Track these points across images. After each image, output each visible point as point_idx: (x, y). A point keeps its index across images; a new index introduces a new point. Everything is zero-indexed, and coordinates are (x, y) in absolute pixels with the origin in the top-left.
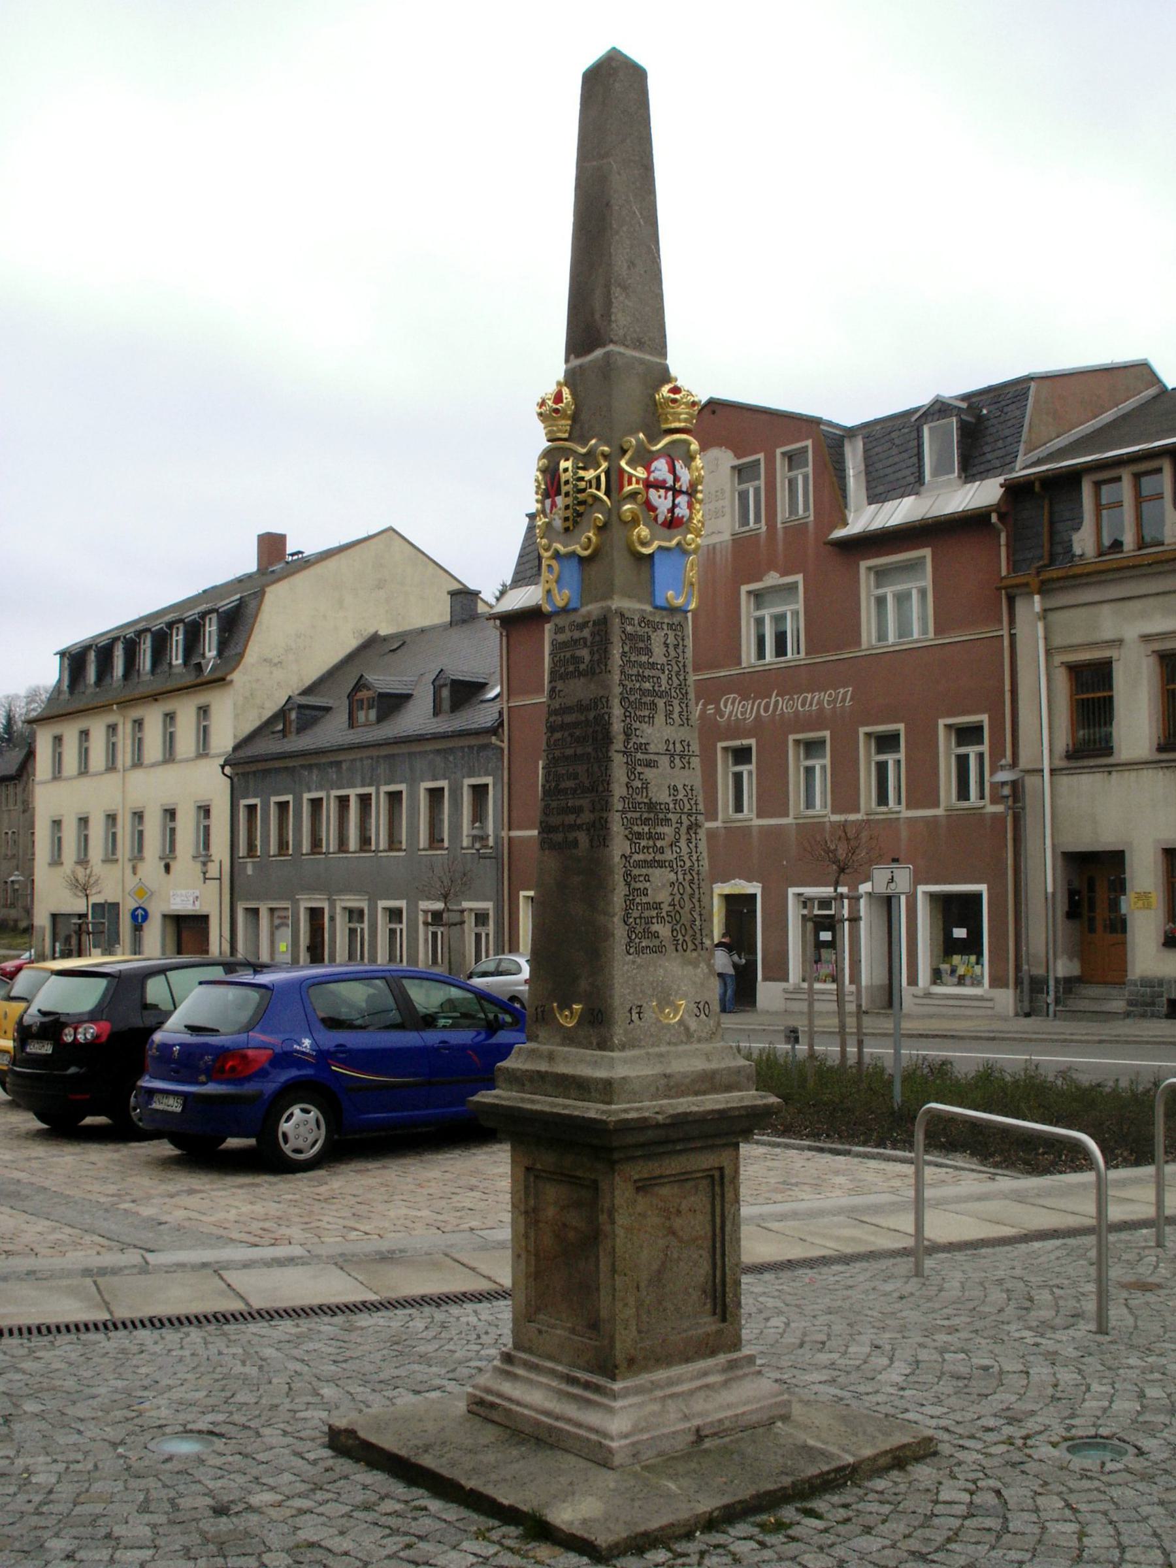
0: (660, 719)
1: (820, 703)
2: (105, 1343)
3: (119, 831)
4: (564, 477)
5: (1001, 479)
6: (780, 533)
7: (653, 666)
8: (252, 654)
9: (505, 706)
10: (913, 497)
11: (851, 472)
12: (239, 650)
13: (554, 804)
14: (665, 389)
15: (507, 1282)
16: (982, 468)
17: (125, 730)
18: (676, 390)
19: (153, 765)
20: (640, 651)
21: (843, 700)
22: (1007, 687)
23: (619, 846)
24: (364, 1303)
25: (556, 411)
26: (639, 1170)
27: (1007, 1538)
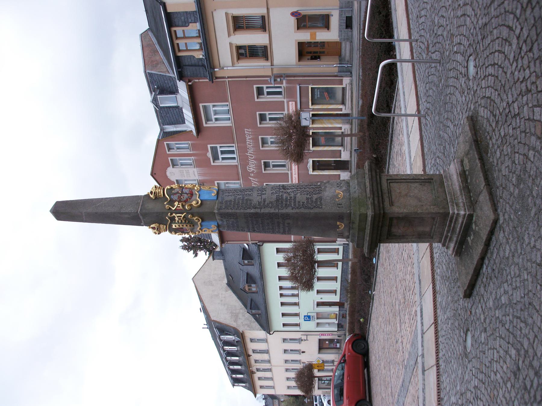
0: (251, 198)
1: (250, 139)
2: (443, 367)
3: (291, 368)
4: (177, 227)
5: (178, 81)
6: (194, 152)
7: (235, 200)
8: (233, 324)
9: (250, 242)
10: (183, 110)
11: (175, 129)
12: (232, 329)
13: (277, 230)
14: (152, 196)
15: (428, 244)
16: (174, 87)
17: (259, 366)
18: (151, 193)
19: (270, 357)
20: (230, 204)
21: (249, 132)
22: (245, 79)
23: (289, 210)
24: (433, 288)
25: (157, 229)
26: (387, 203)
27: (492, 98)
